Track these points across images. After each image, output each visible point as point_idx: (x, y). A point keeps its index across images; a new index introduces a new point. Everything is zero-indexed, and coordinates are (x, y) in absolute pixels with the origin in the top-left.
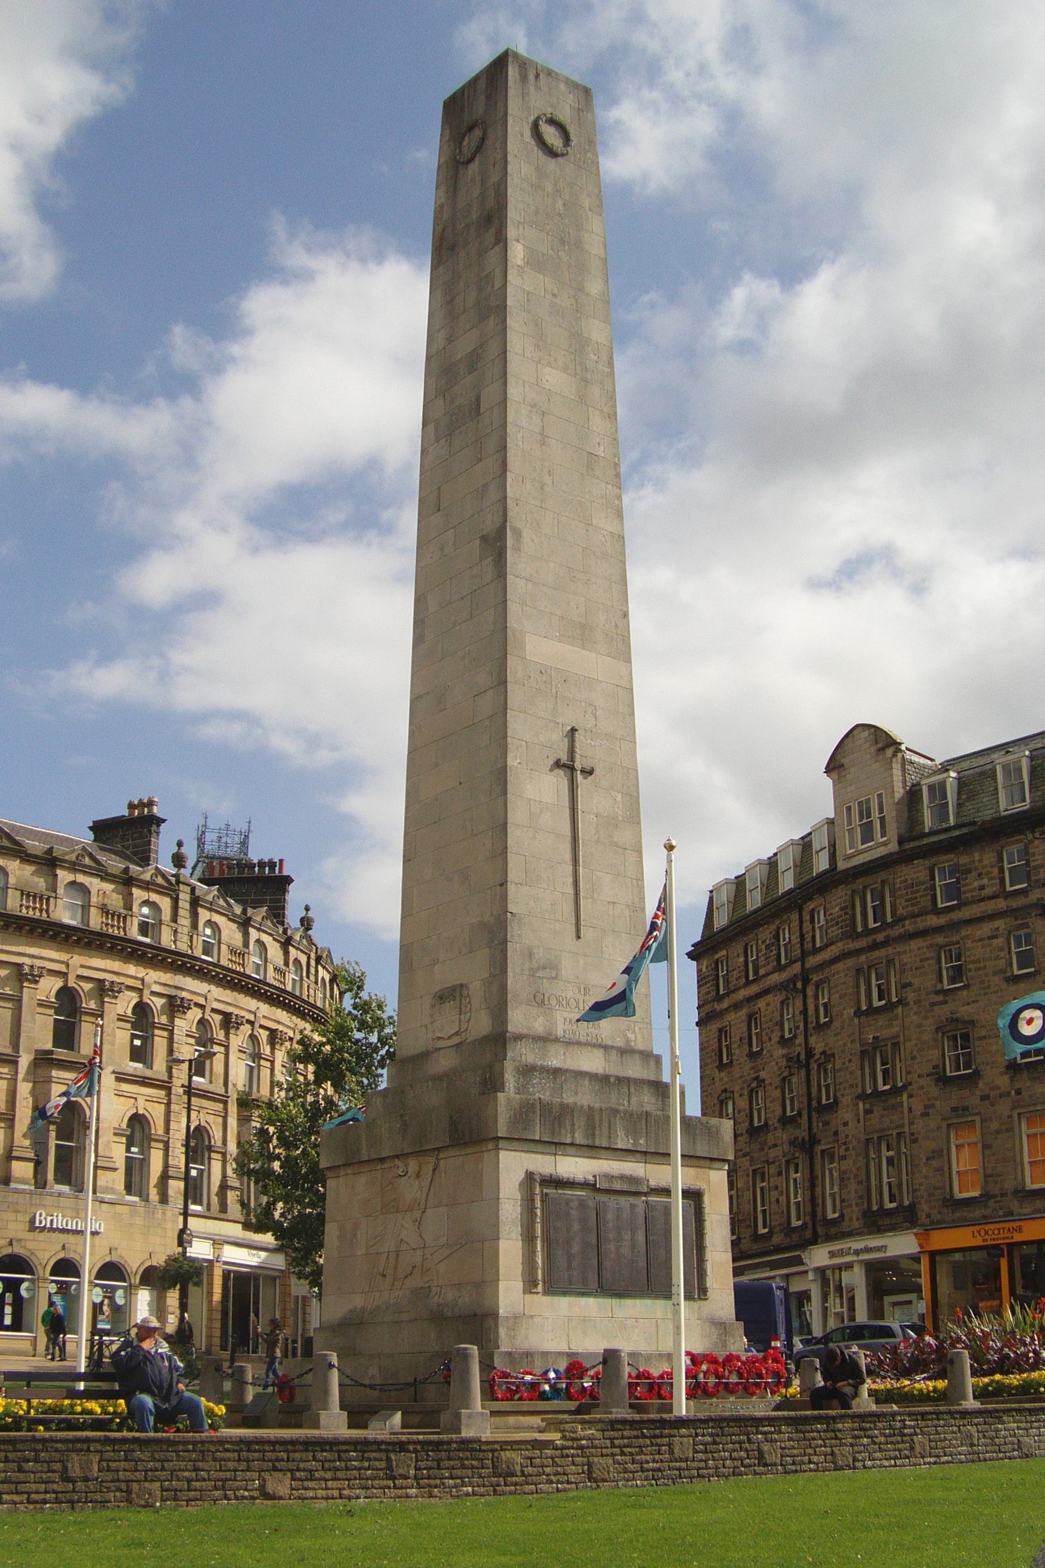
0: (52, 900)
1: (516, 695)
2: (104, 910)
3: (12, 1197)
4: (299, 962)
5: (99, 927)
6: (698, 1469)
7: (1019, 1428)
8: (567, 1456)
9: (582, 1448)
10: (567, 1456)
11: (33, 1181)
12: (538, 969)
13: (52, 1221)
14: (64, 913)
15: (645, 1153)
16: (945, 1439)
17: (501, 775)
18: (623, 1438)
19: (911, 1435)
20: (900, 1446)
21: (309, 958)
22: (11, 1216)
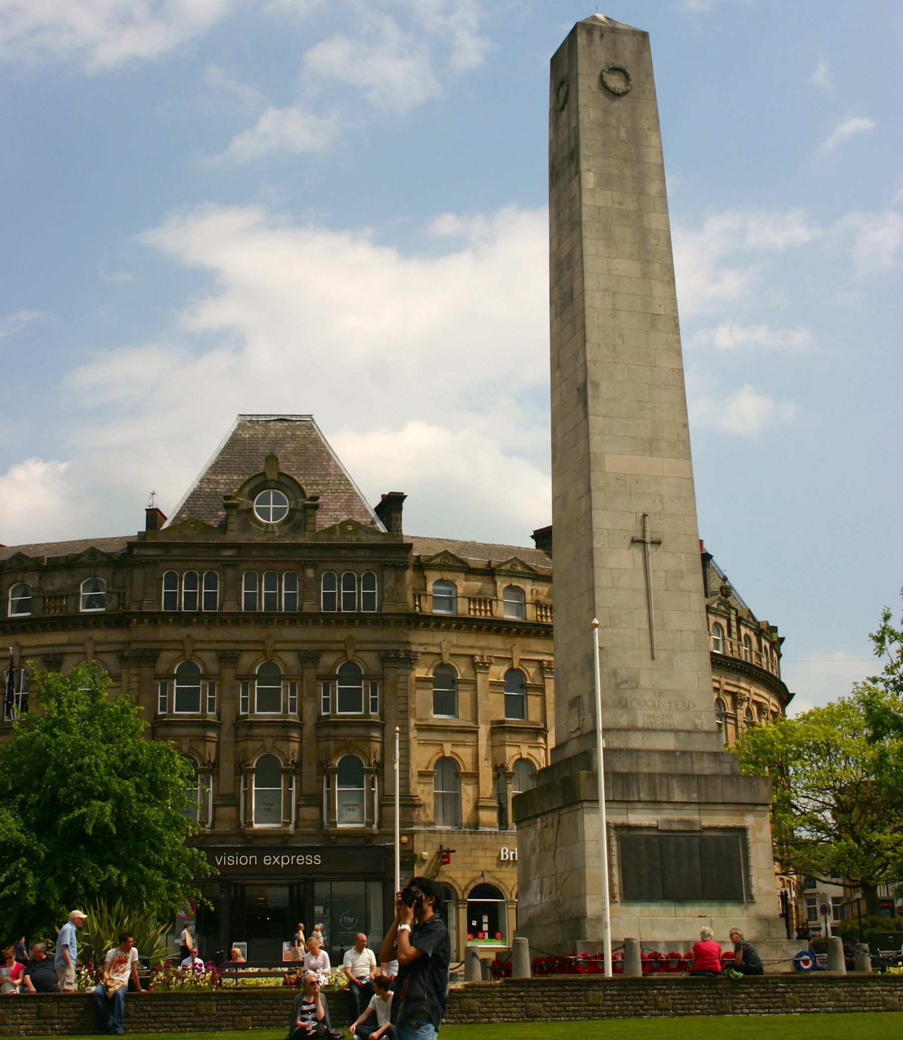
0: (494, 603)
1: (598, 498)
2: (538, 604)
3: (480, 838)
4: (720, 624)
5: (535, 619)
6: (607, 1011)
7: (883, 990)
8: (511, 1002)
9: (521, 997)
10: (511, 1002)
11: (497, 825)
12: (622, 683)
13: (514, 855)
14: (504, 612)
15: (699, 803)
16: (814, 996)
17: (591, 552)
18: (550, 991)
19: (783, 993)
20: (774, 1000)
21: (729, 620)
22: (480, 853)
